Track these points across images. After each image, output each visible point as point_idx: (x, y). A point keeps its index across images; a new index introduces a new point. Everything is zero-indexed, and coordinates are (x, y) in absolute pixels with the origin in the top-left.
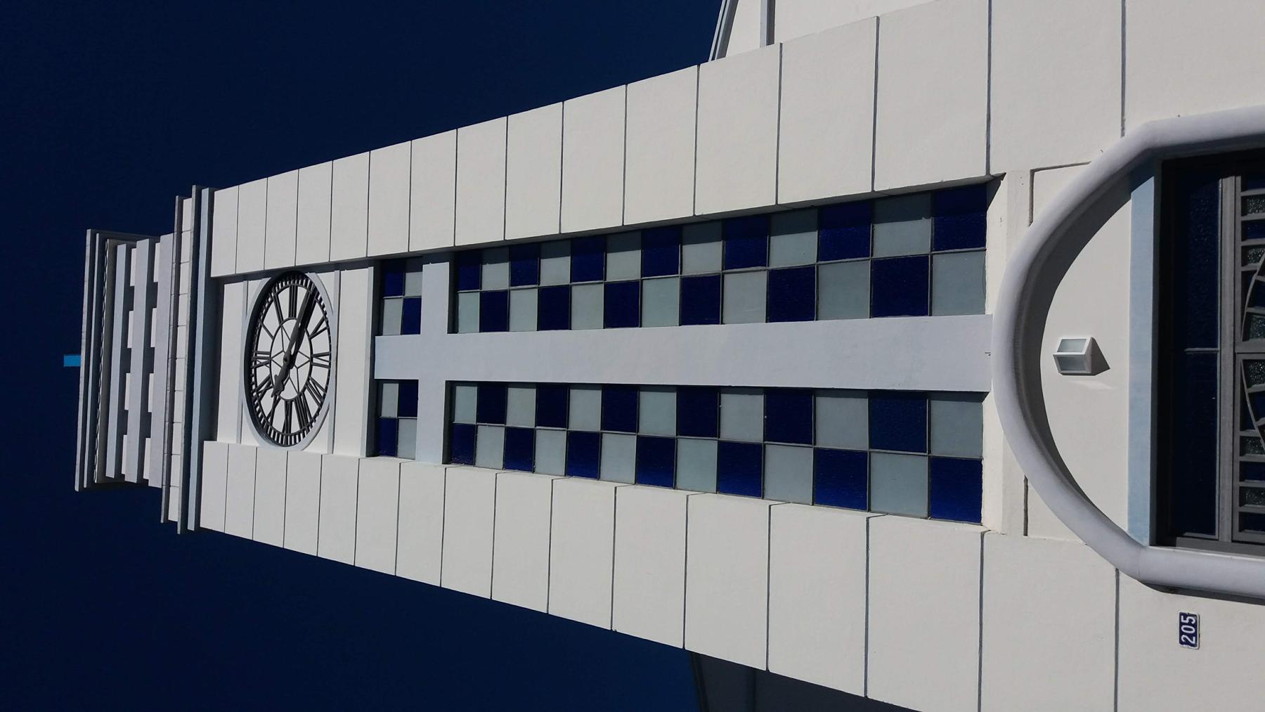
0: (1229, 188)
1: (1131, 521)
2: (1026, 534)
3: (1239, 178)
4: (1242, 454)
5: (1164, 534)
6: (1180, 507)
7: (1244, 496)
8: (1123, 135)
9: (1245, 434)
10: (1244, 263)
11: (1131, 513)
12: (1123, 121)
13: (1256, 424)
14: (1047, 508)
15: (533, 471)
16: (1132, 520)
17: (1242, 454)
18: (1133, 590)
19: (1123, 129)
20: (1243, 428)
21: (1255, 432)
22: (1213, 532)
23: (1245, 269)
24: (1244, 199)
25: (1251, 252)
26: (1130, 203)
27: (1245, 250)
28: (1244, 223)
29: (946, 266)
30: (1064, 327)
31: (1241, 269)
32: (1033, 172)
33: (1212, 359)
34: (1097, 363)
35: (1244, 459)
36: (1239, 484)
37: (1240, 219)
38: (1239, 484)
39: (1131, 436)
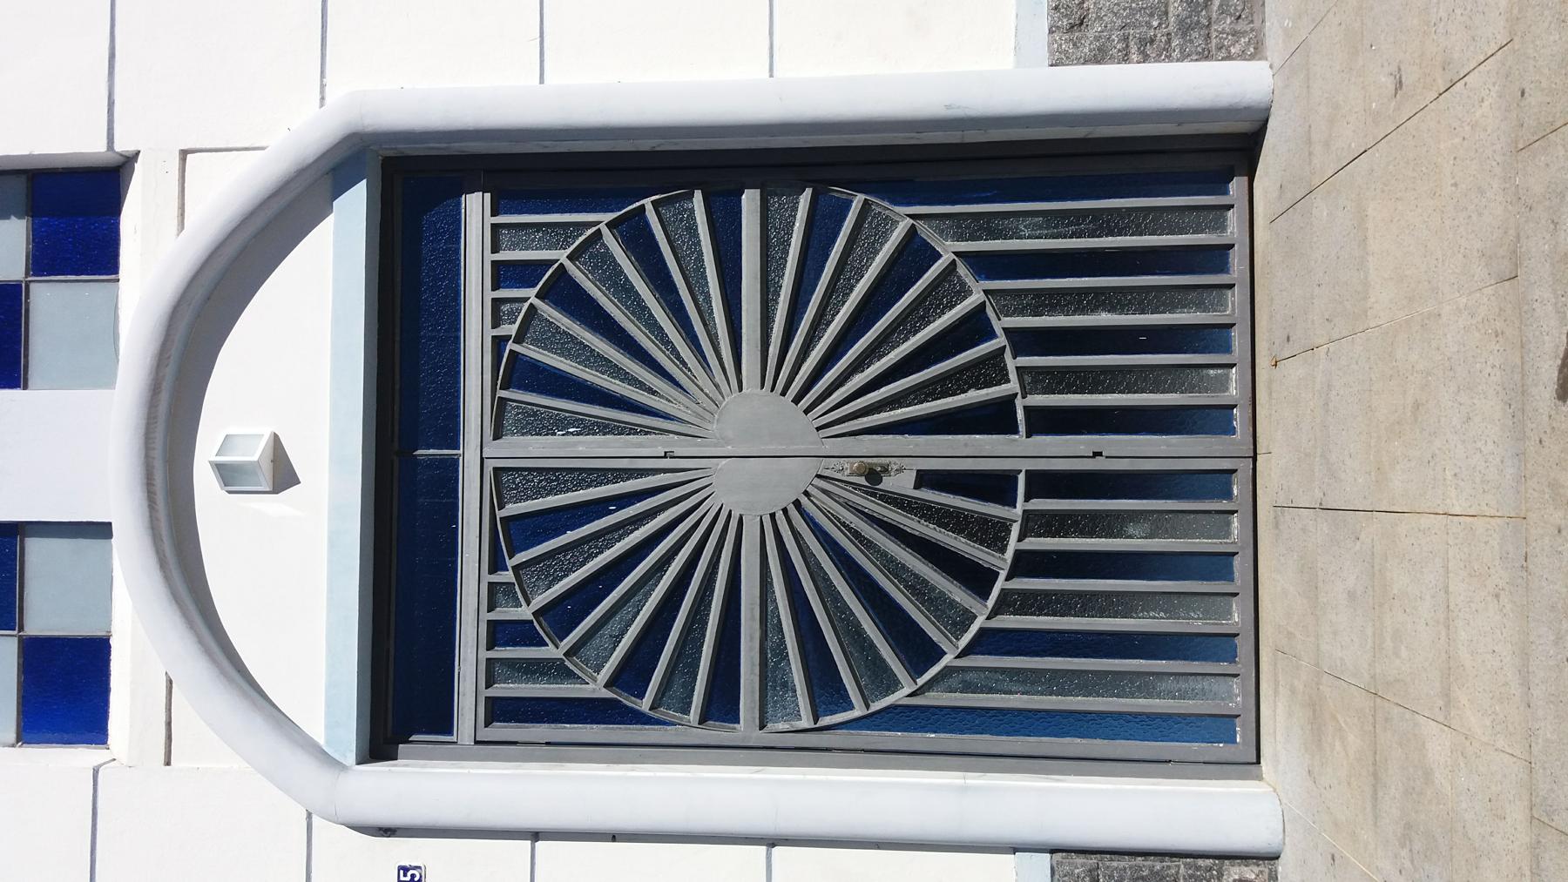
0: (475, 208)
1: (328, 727)
2: (168, 763)
3: (488, 196)
4: (495, 250)
5: (380, 744)
6: (403, 702)
7: (492, 671)
8: (322, 105)
9: (495, 578)
10: (495, 325)
11: (328, 714)
12: (323, 86)
13: (510, 563)
14: (204, 704)
15: (25, 388)
16: (330, 726)
17: (495, 250)
18: (335, 841)
19: (323, 98)
20: (492, 571)
21: (507, 576)
22: (450, 733)
23: (497, 332)
24: (497, 302)
25: (505, 308)
26: (330, 220)
27: (497, 302)
28: (492, 624)
29: (53, 306)
30: (231, 417)
31: (490, 333)
32: (184, 154)
33: (450, 469)
34: (283, 474)
35: (493, 616)
36: (485, 654)
37: (490, 257)
38: (485, 654)
39: (330, 590)
